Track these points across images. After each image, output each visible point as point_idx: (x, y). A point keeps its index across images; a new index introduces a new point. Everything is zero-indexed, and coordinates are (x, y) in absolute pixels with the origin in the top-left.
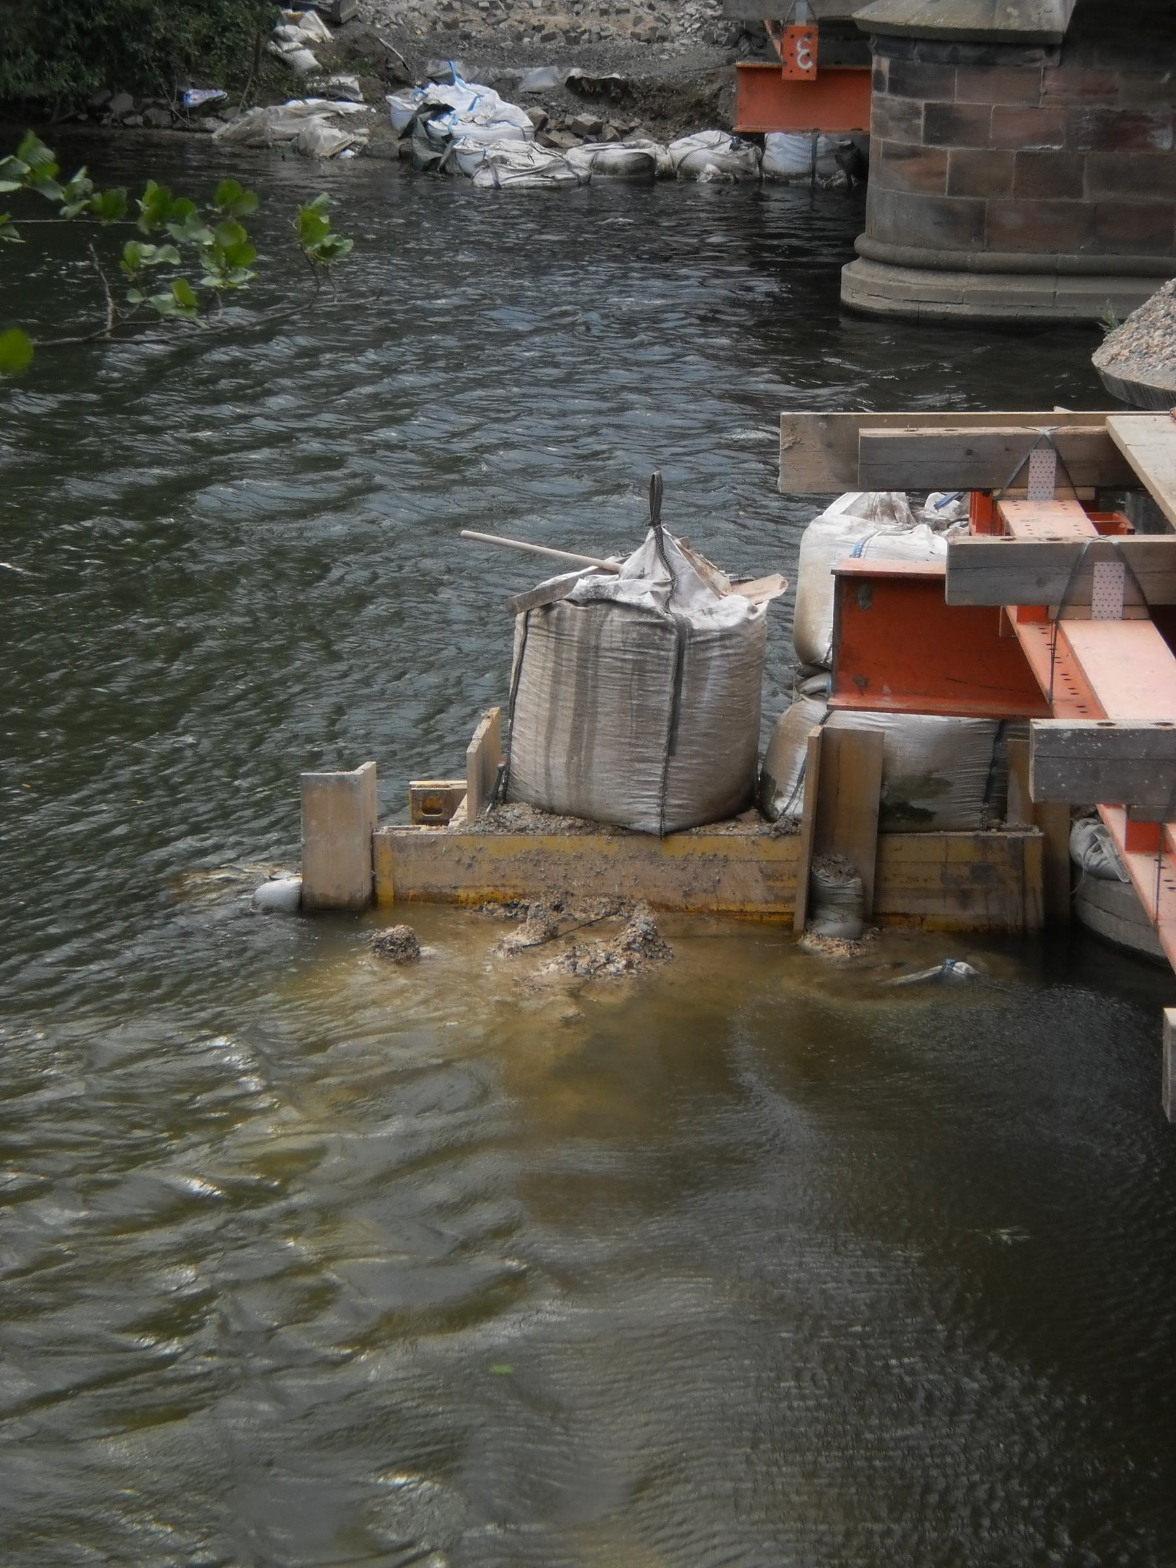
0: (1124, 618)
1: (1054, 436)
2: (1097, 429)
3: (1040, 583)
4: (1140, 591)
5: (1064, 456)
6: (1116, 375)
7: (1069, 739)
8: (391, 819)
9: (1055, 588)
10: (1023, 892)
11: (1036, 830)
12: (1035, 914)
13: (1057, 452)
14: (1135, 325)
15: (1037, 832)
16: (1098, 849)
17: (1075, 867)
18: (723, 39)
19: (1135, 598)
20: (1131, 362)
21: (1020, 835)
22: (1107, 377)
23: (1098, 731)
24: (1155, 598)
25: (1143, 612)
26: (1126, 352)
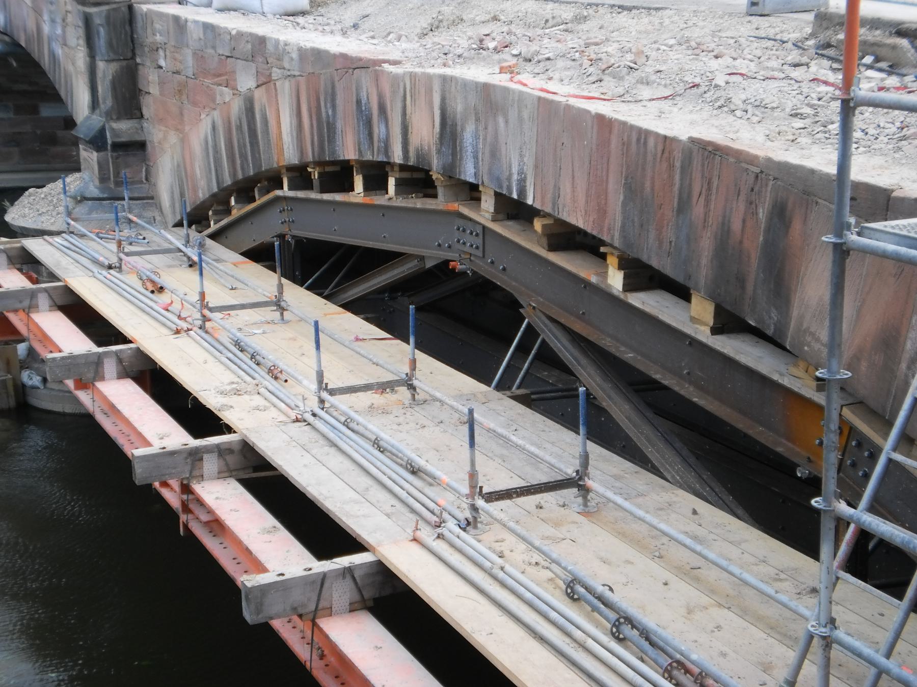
0: (50, 311)
1: (5, 248)
2: (18, 245)
3: (21, 302)
4: (54, 301)
5: (9, 255)
6: (16, 224)
7: (59, 360)
8: (77, 514)
9: (26, 303)
10: (8, 397)
11: (9, 375)
12: (12, 403)
13: (6, 253)
14: (17, 207)
15: (10, 376)
16: (31, 379)
17: (24, 386)
18: (74, 206)
19: (53, 304)
20: (19, 220)
21: (4, 378)
22: (12, 225)
23: (69, 356)
24: (59, 303)
25: (56, 308)
26: (17, 216)
